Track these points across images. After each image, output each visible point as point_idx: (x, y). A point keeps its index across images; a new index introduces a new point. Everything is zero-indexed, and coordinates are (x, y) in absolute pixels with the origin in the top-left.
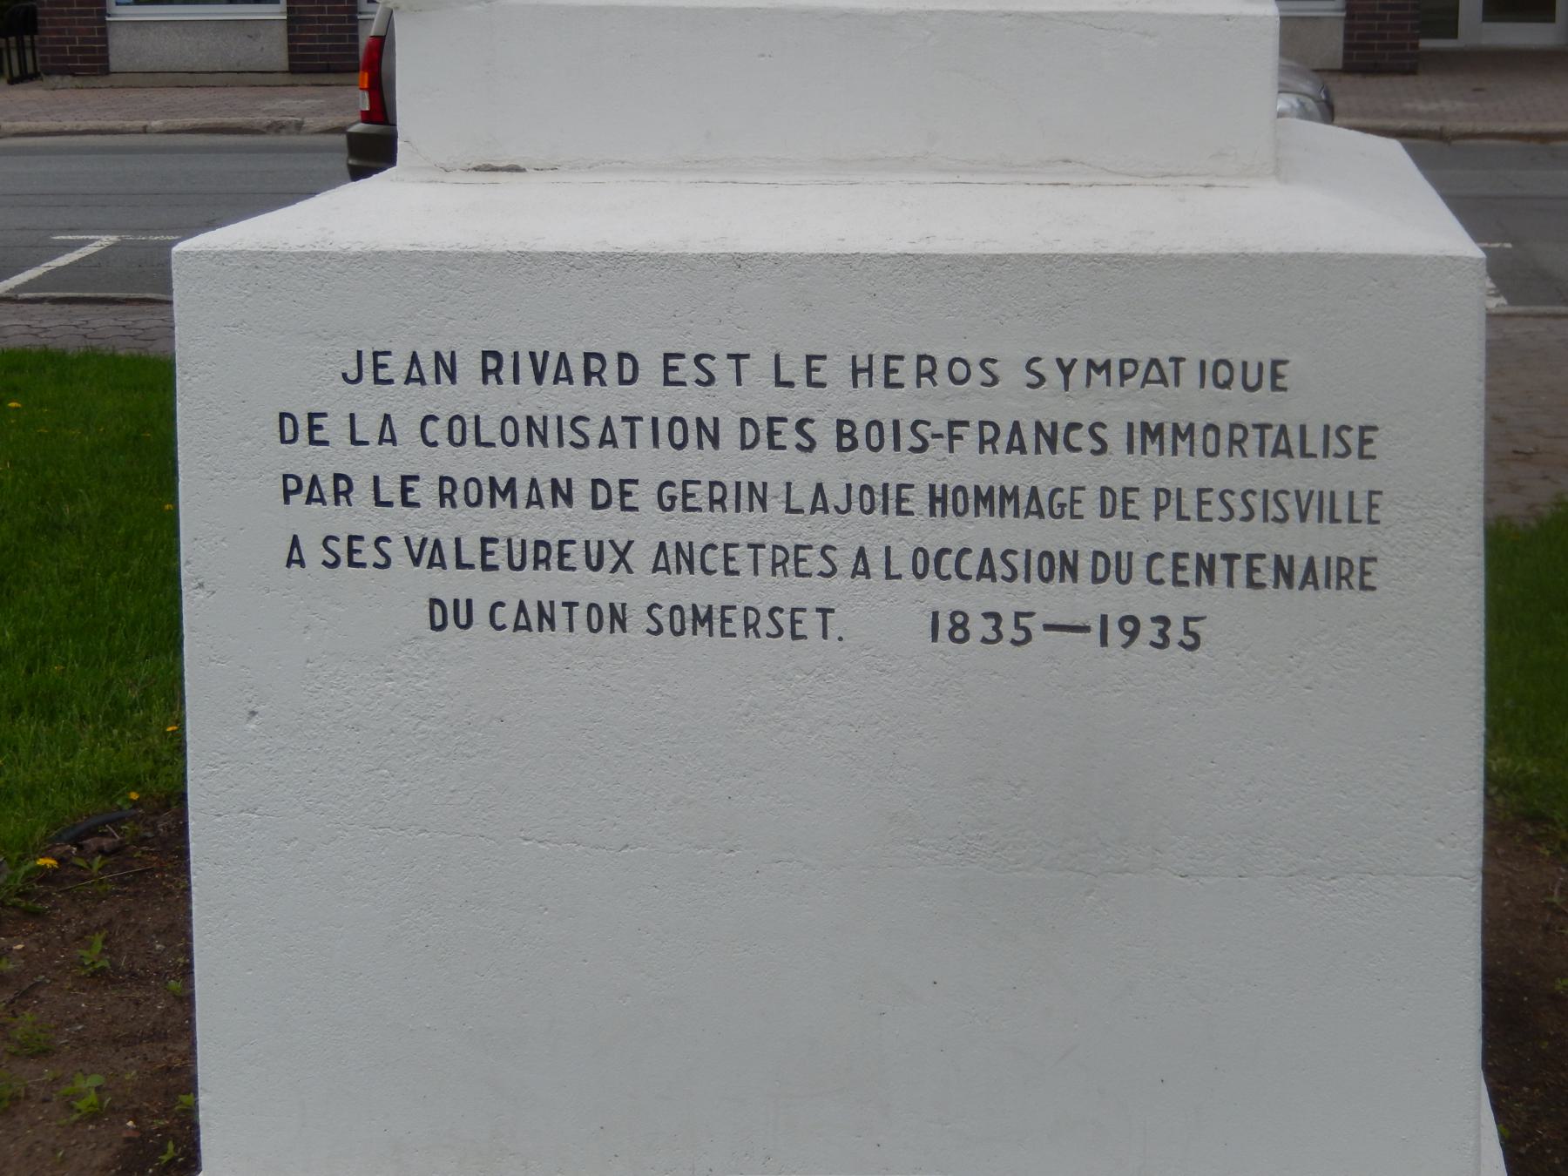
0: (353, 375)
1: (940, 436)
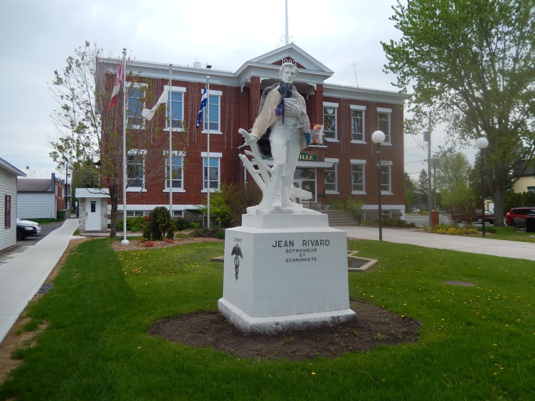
0: (275, 245)
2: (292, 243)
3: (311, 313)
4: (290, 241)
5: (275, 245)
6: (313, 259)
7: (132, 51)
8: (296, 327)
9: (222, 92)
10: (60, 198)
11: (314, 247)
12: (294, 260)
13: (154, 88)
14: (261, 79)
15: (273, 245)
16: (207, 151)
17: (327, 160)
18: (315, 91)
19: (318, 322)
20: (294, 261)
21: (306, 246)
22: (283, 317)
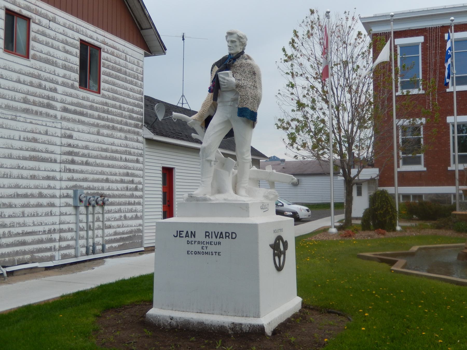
0: (176, 235)
1: (51, 235)
2: (193, 234)
3: (213, 314)
4: (192, 232)
6: (217, 254)
7: (355, 8)
8: (191, 326)
11: (218, 240)
12: (195, 253)
13: (432, 40)
15: (174, 235)
16: (453, 115)
19: (214, 326)
20: (195, 254)
21: (209, 238)
22: (182, 312)
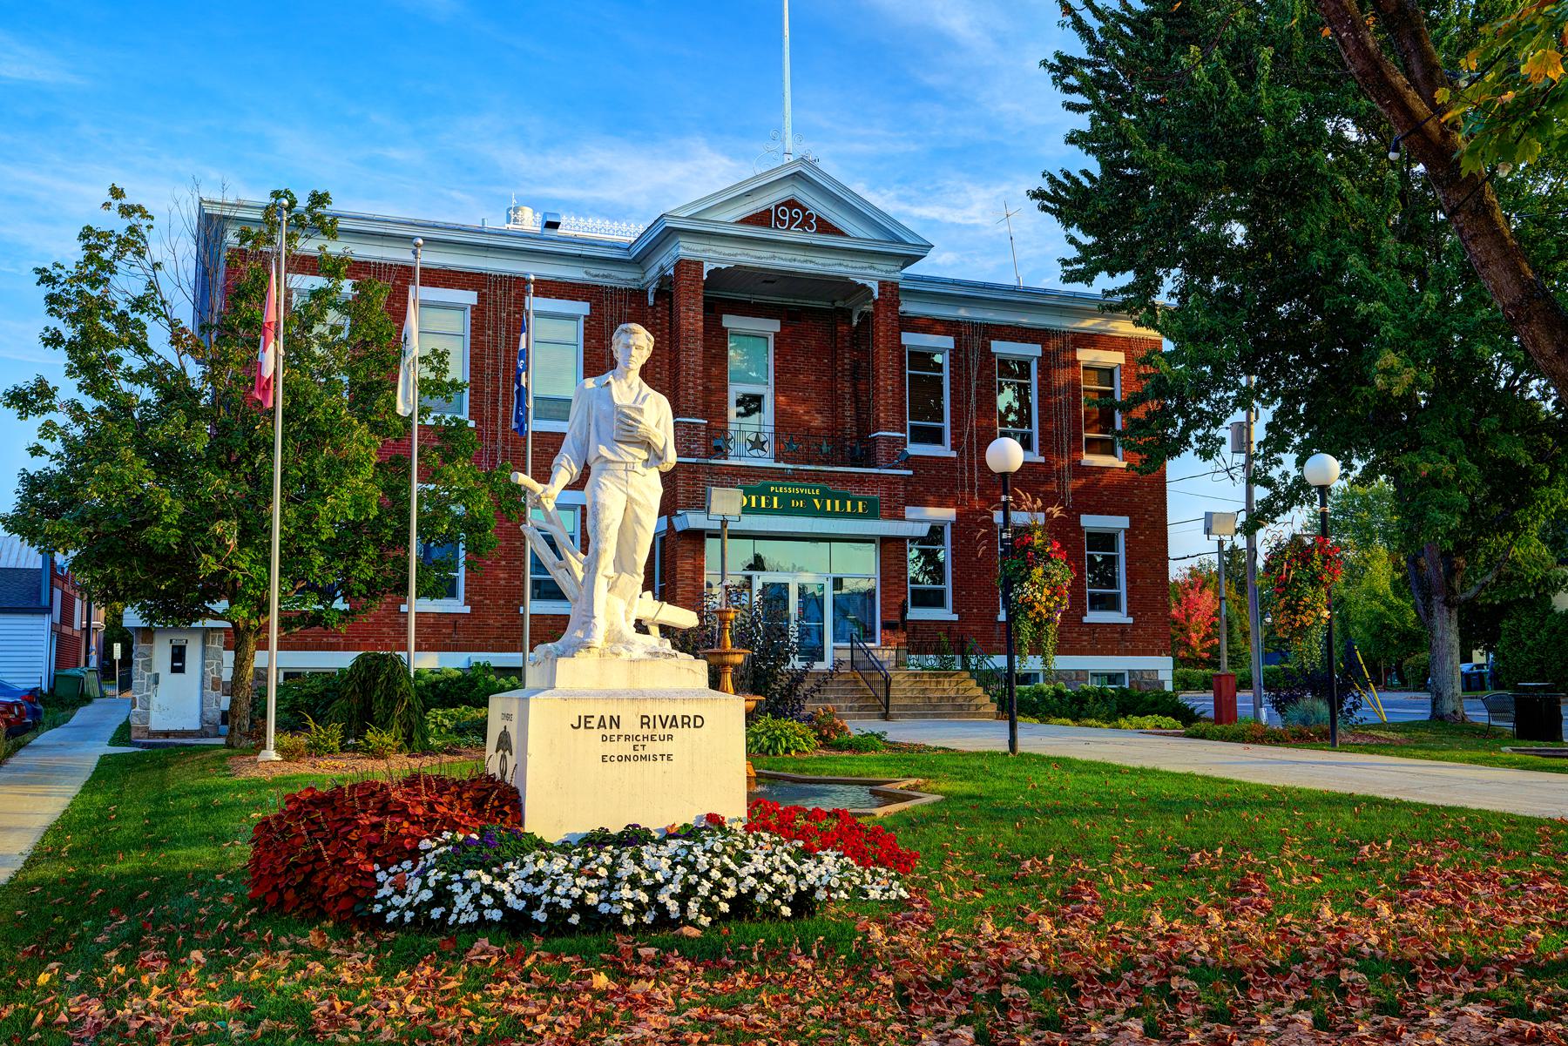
0: (576, 725)
5: (576, 725)
9: (587, 304)
10: (66, 630)
11: (667, 731)
14: (707, 267)
17: (911, 512)
18: (875, 302)
